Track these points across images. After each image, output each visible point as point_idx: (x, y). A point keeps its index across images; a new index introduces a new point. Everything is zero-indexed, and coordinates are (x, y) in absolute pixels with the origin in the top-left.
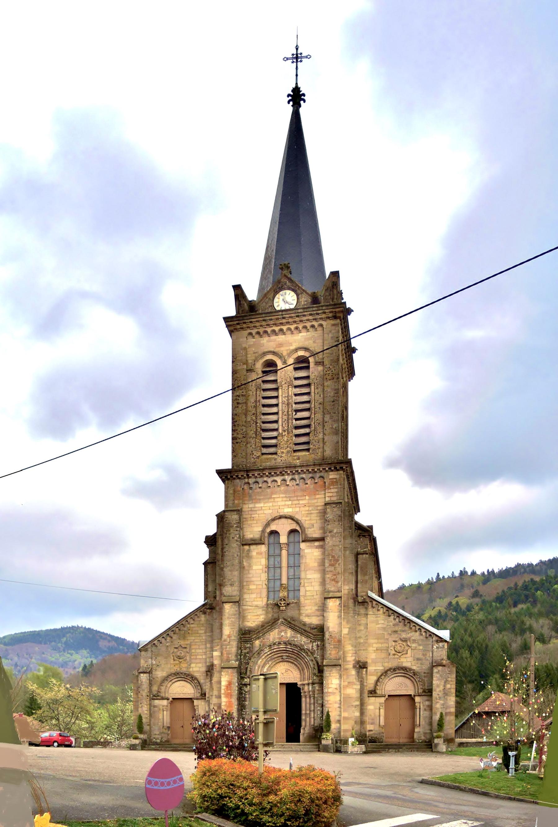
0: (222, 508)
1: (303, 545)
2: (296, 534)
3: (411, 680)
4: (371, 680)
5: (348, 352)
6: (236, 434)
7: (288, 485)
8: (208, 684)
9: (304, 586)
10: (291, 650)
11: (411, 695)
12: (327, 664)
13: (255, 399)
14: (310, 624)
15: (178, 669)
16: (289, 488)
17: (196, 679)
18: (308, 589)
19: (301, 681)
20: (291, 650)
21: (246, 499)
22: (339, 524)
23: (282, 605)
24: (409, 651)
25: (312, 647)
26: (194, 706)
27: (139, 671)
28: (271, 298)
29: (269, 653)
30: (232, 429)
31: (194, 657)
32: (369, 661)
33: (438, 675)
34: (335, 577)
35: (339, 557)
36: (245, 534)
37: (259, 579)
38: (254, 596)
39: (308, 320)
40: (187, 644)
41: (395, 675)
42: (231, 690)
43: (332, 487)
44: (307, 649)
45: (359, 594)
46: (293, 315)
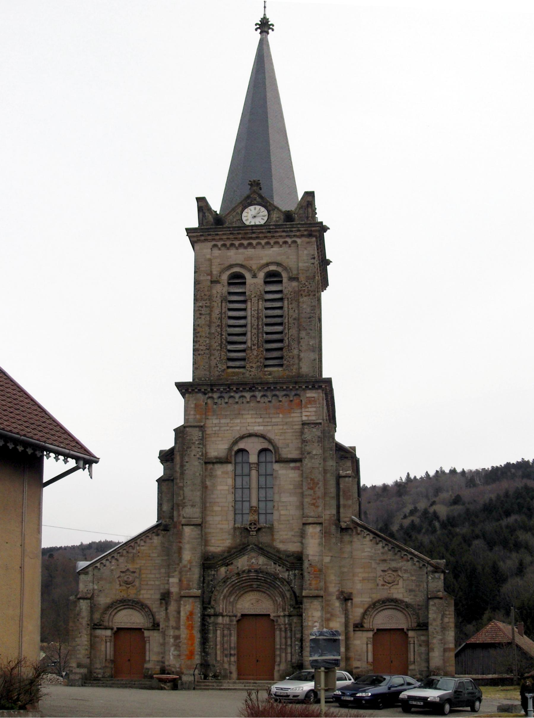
0: (180, 422)
1: (276, 466)
2: (268, 454)
3: (404, 613)
4: (357, 613)
5: (322, 265)
6: (198, 345)
7: (259, 401)
8: (163, 613)
10: (263, 579)
11: (403, 629)
12: (306, 595)
13: (220, 311)
14: (285, 551)
15: (125, 596)
16: (260, 405)
17: (147, 606)
18: (283, 512)
19: (274, 613)
20: (263, 579)
21: (210, 414)
22: (319, 445)
24: (401, 582)
25: (289, 575)
26: (145, 637)
27: (78, 596)
28: (239, 212)
29: (236, 581)
30: (193, 340)
31: (145, 583)
32: (355, 592)
33: (434, 608)
34: (314, 501)
36: (208, 451)
38: (218, 518)
39: (281, 236)
40: (136, 568)
41: (385, 607)
43: (308, 406)
44: (282, 578)
45: (341, 520)
46: (264, 231)
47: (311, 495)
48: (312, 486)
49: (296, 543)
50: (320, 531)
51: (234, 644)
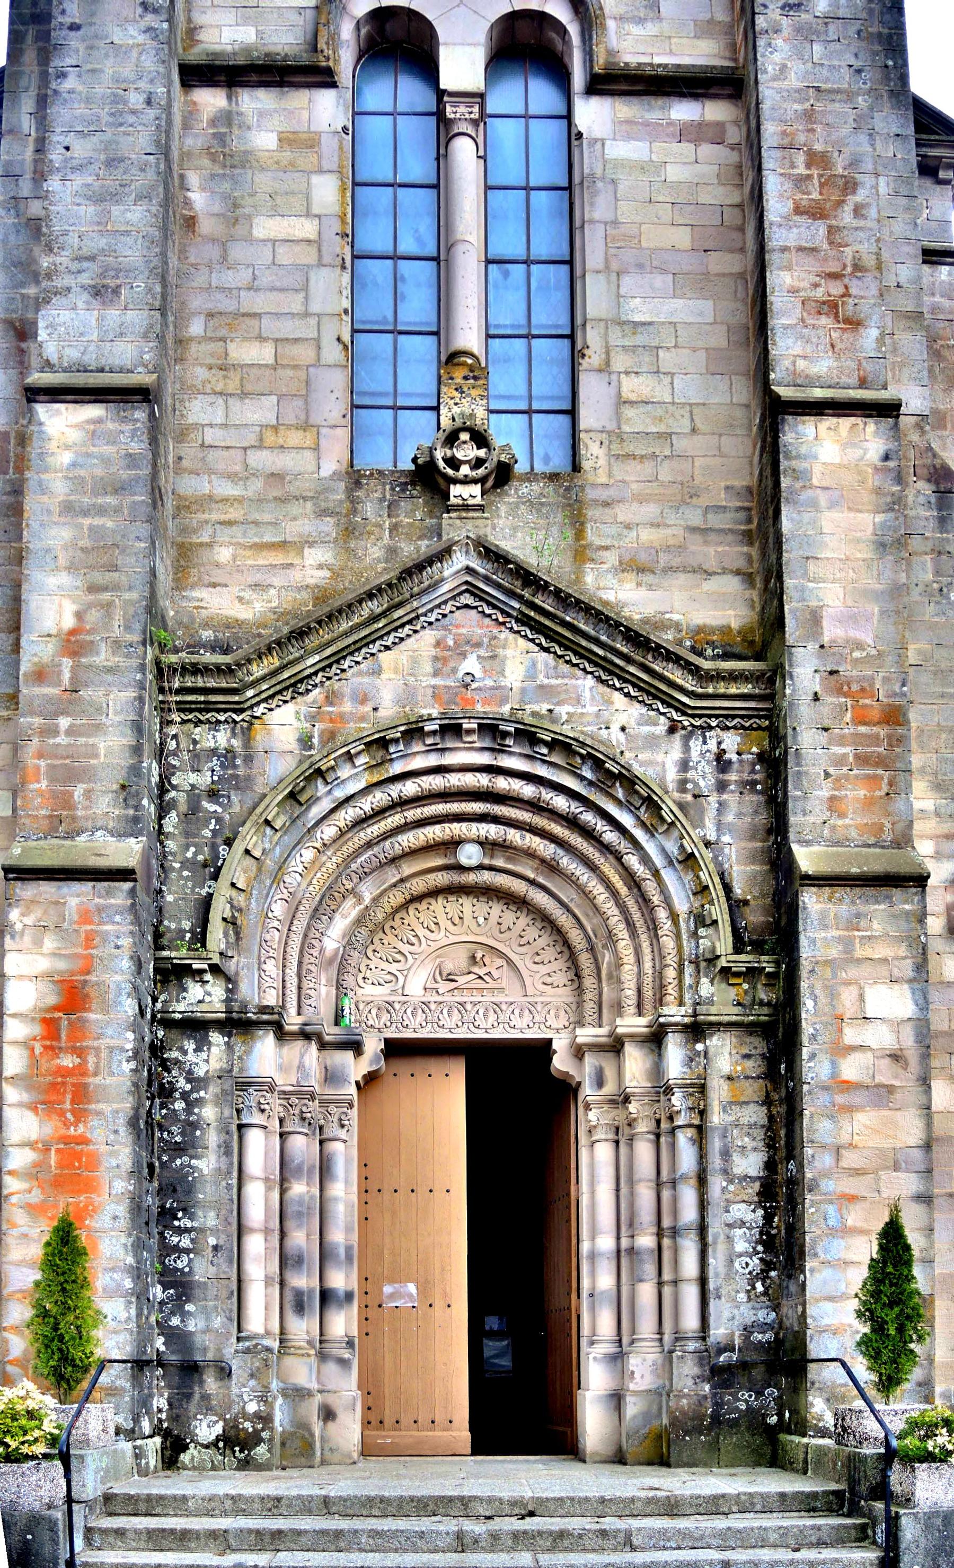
9: (605, 368)
18: (632, 387)
20: (528, 791)
23: (465, 470)
25: (684, 765)
34: (836, 289)
35: (854, 163)
37: (295, 303)
42: (80, 1052)
47: (814, 250)
48: (815, 195)
49: (709, 574)
50: (886, 458)
51: (348, 1230)
